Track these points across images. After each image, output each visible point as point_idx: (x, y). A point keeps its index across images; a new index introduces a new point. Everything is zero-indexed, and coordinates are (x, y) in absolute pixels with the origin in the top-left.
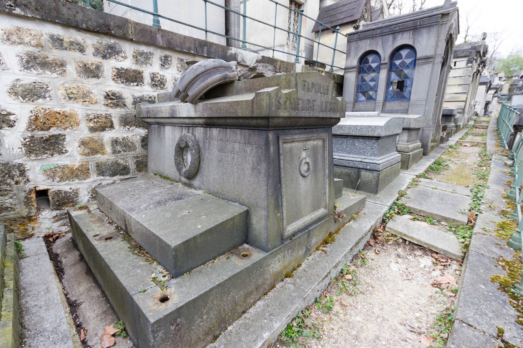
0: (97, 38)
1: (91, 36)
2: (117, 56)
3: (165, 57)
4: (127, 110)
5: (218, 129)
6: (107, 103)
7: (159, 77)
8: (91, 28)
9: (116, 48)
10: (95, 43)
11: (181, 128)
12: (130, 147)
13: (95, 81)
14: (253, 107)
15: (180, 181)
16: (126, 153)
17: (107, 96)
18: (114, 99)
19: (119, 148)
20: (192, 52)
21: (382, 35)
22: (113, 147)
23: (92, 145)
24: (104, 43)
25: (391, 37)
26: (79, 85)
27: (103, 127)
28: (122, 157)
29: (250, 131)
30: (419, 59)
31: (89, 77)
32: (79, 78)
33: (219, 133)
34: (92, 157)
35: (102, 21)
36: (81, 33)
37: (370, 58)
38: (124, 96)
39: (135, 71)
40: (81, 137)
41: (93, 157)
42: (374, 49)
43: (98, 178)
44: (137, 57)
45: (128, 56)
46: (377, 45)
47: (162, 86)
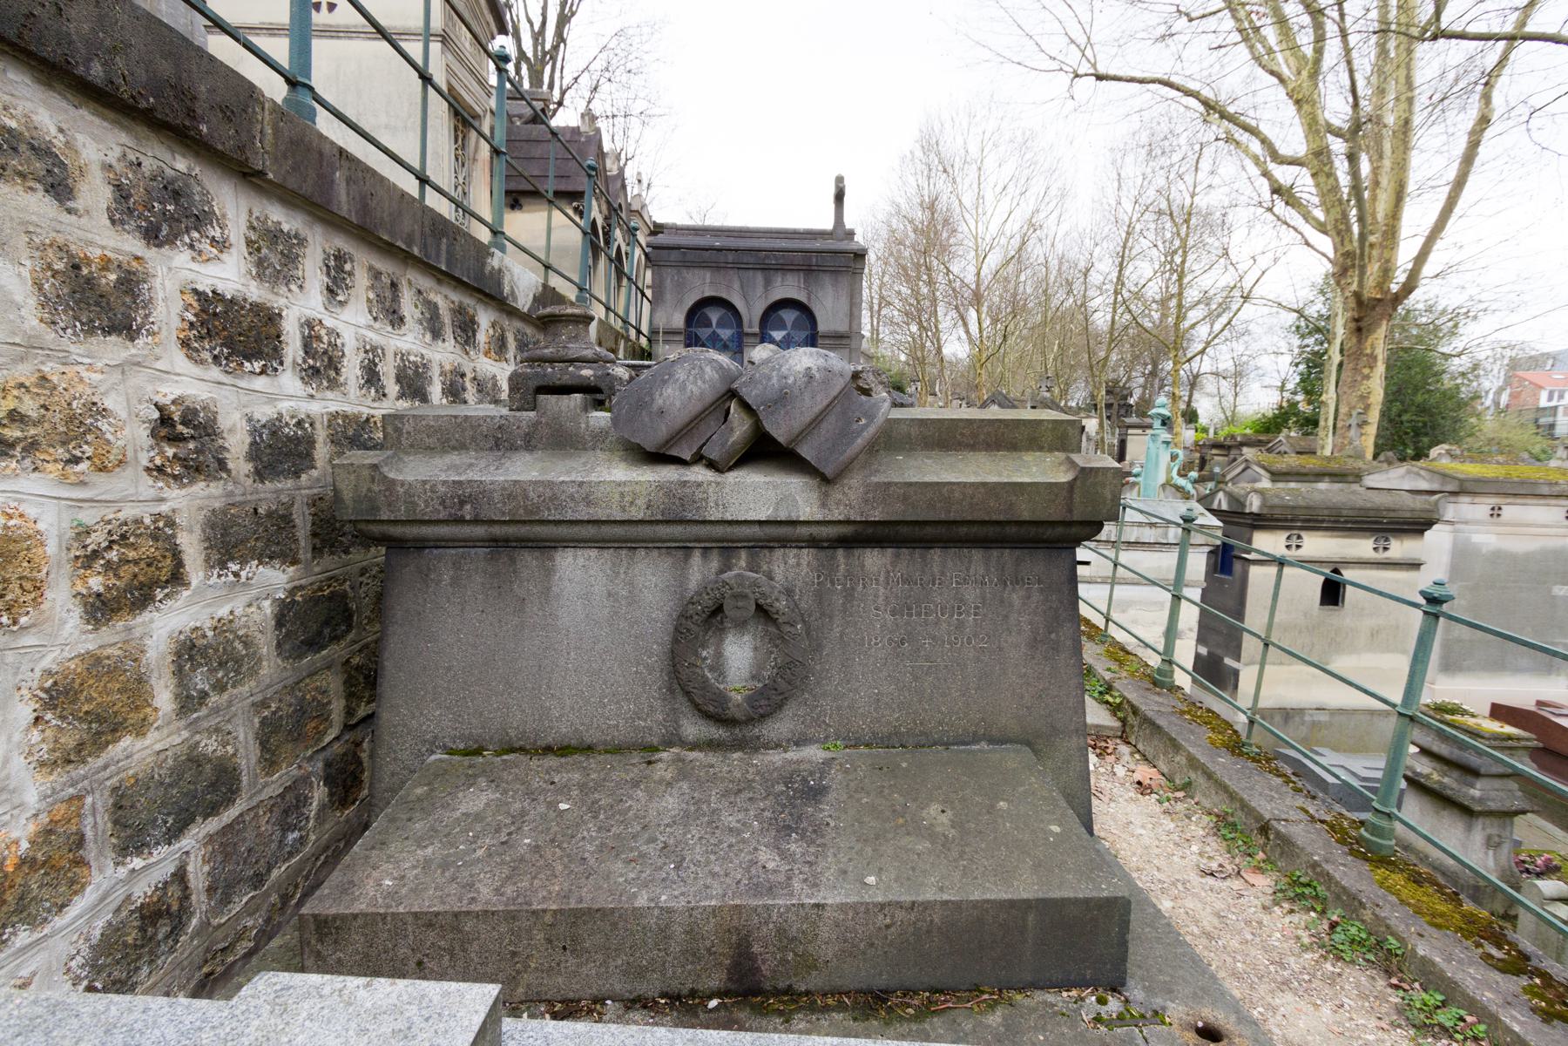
0: (124, 138)
1: (97, 121)
2: (196, 235)
3: (336, 257)
4: (230, 487)
5: (890, 550)
6: (158, 461)
7: (325, 339)
8: (125, 92)
9: (190, 196)
10: (112, 158)
11: (680, 553)
12: (238, 661)
13: (113, 349)
14: (1071, 498)
15: (673, 740)
16: (225, 696)
17: (166, 426)
18: (183, 436)
19: (200, 680)
20: (416, 251)
21: (739, 267)
22: (180, 684)
23: (94, 697)
24: (149, 165)
25: (759, 277)
26: (46, 369)
27: (142, 586)
28: (213, 722)
29: (1018, 552)
30: (824, 337)
31: (91, 331)
32: (50, 336)
33: (893, 564)
34: (95, 763)
35: (165, 68)
36: (56, 100)
37: (714, 315)
38: (224, 423)
39: (257, 308)
40: (47, 663)
41: (100, 762)
42: (724, 296)
43: (122, 872)
44: (259, 250)
45: (232, 239)
46: (729, 287)
47: (332, 373)
